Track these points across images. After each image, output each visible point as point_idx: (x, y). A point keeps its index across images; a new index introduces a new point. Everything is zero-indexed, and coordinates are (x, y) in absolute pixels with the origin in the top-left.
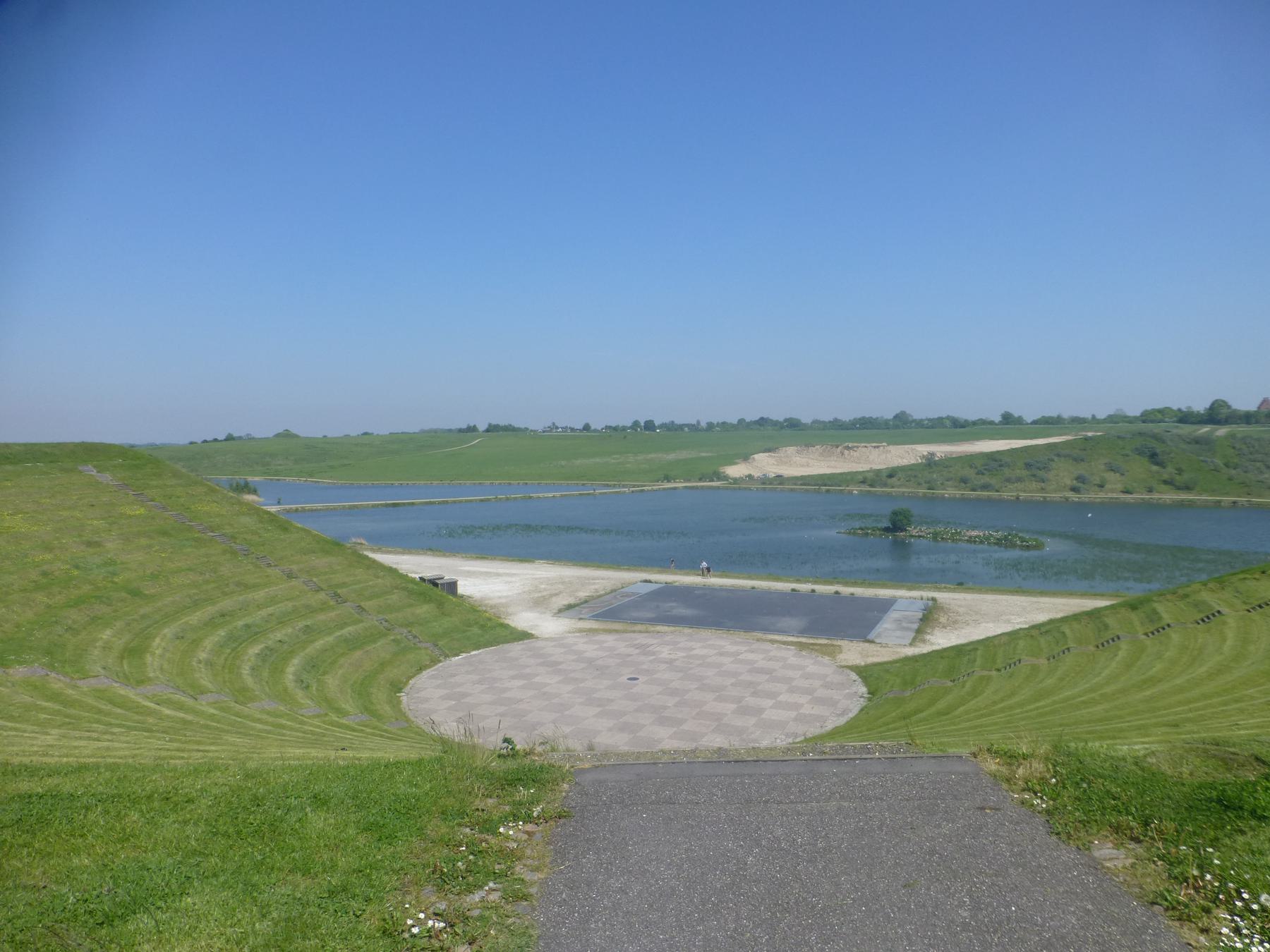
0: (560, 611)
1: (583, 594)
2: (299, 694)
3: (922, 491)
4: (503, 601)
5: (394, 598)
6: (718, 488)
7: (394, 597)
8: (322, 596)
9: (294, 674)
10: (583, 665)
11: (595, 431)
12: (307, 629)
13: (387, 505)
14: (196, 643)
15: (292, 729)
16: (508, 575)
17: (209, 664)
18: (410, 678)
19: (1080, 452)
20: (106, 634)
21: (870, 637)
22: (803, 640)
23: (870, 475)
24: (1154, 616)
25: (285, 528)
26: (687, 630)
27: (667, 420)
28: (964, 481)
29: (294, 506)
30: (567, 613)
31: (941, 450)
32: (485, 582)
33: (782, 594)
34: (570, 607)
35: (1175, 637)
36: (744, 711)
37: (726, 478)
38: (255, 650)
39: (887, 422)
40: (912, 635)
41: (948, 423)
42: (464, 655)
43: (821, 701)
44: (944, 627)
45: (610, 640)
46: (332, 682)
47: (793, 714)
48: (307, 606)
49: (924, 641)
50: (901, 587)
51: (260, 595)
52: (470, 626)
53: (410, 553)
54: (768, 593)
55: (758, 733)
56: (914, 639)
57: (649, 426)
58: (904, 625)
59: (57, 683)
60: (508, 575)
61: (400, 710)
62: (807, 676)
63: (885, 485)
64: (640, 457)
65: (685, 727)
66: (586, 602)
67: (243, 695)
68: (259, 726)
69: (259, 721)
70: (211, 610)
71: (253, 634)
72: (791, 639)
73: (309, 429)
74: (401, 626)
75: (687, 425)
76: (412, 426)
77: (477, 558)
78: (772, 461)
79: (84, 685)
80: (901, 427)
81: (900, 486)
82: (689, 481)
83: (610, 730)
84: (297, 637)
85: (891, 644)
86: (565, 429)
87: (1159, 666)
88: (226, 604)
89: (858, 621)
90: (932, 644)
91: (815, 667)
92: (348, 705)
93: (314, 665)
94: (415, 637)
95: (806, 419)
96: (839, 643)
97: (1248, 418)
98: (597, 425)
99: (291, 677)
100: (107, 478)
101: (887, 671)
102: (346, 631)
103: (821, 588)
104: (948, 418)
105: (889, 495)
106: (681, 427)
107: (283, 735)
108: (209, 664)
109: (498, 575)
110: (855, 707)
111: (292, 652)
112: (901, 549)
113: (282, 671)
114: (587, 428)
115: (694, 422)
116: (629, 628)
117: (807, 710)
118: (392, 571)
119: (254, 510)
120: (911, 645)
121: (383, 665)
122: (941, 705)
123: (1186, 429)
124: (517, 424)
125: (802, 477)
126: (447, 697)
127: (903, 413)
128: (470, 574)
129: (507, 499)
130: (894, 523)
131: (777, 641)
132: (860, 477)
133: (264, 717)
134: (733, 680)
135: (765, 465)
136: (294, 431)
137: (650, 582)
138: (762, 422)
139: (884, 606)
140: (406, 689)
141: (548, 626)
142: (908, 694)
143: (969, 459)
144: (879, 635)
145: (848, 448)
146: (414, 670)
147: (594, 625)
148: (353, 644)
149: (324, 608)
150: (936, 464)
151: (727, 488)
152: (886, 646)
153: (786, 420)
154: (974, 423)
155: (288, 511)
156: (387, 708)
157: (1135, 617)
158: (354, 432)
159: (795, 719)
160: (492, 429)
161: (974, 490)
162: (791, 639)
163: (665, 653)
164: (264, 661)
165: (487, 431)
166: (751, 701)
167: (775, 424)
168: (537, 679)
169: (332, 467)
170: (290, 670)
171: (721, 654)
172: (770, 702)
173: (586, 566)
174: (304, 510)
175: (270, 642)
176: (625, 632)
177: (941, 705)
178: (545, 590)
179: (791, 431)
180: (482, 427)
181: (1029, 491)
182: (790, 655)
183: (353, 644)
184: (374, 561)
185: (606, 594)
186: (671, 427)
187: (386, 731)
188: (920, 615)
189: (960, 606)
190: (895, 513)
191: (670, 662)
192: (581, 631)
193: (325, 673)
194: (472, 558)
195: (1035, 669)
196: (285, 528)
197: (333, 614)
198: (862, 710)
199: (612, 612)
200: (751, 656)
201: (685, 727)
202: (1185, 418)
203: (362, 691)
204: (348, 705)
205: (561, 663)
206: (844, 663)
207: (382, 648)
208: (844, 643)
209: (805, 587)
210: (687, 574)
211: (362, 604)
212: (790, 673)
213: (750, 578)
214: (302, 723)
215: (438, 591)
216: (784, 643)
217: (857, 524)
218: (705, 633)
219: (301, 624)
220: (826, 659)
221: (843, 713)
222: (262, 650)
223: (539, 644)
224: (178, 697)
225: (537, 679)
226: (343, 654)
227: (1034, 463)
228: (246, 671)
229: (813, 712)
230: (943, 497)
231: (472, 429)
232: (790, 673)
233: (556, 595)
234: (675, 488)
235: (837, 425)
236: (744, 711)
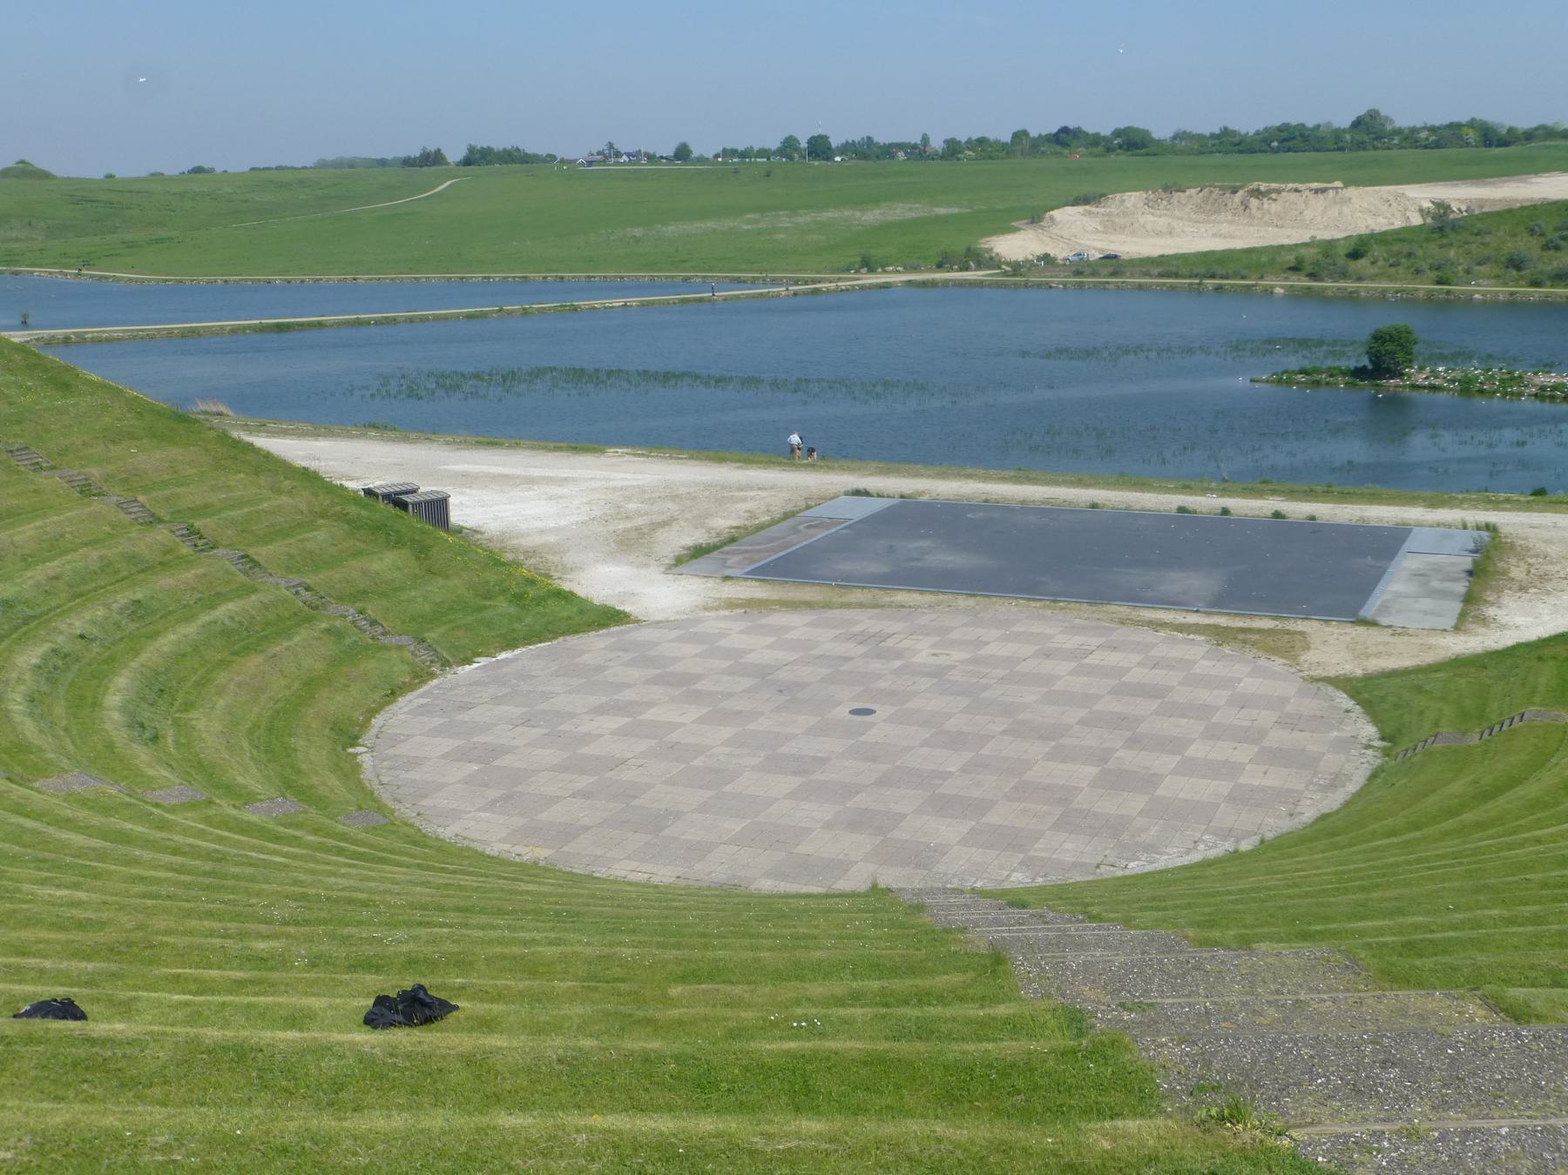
0: (679, 561)
1: (723, 523)
2: (142, 755)
3: (1424, 287)
4: (552, 539)
5: (321, 536)
6: (979, 284)
7: (321, 535)
8: (161, 534)
9: (123, 709)
10: (747, 682)
11: (702, 160)
12: (137, 610)
13: (262, 329)
15: (147, 844)
16: (550, 480)
18: (373, 712)
21: (1367, 611)
22: (1222, 621)
23: (1309, 254)
25: (63, 383)
26: (963, 602)
27: (856, 136)
28: (1516, 263)
29: (60, 332)
30: (697, 564)
31: (1461, 196)
32: (509, 497)
33: (1157, 519)
34: (698, 552)
36: (1116, 781)
37: (993, 262)
38: (29, 657)
39: (1338, 135)
40: (1457, 606)
41: (1471, 135)
42: (483, 661)
44: (1523, 589)
45: (797, 624)
46: (207, 725)
47: (1225, 787)
48: (132, 558)
49: (1484, 621)
50: (1411, 501)
52: (488, 596)
53: (329, 434)
54: (1129, 517)
55: (1154, 830)
56: (1462, 616)
57: (819, 148)
58: (1435, 584)
60: (550, 480)
61: (361, 786)
62: (1243, 702)
63: (1344, 275)
64: (805, 218)
65: (993, 818)
66: (733, 540)
68: (78, 839)
69: (68, 823)
72: (1193, 619)
74: (340, 599)
75: (900, 146)
76: (301, 153)
77: (478, 444)
78: (1092, 224)
80: (1367, 147)
81: (1372, 278)
82: (915, 268)
83: (828, 826)
84: (118, 625)
85: (1413, 627)
86: (635, 156)
89: (1337, 578)
90: (1503, 627)
91: (1254, 677)
93: (158, 688)
94: (373, 623)
95: (1161, 131)
96: (1300, 626)
99: (116, 716)
101: (1419, 689)
102: (226, 610)
103: (1242, 506)
104: (1472, 124)
105: (1351, 298)
106: (889, 151)
107: (135, 862)
109: (530, 481)
110: (1357, 769)
111: (110, 660)
112: (1392, 416)
113: (96, 704)
114: (682, 153)
115: (917, 140)
116: (835, 596)
117: (1253, 777)
118: (309, 477)
120: (1457, 628)
121: (311, 685)
124: (530, 148)
125: (1162, 260)
126: (462, 755)
127: (1373, 115)
129: (525, 312)
130: (1376, 358)
131: (1164, 625)
132: (1290, 259)
133: (82, 814)
134: (1082, 713)
135: (1075, 232)
136: (40, 162)
137: (866, 493)
138: (1065, 138)
139: (1389, 542)
140: (368, 738)
141: (659, 595)
142: (1474, 740)
143: (1529, 217)
144: (1384, 609)
145: (1257, 193)
146: (377, 696)
147: (757, 591)
148: (241, 639)
149: (166, 561)
150: (1456, 226)
151: (998, 285)
152: (1403, 632)
153: (1118, 133)
154: (1529, 136)
155: (49, 343)
156: (333, 781)
158: (174, 164)
159: (1231, 799)
160: (477, 158)
161: (1536, 284)
162: (1193, 619)
163: (923, 652)
164: (52, 681)
165: (467, 162)
166: (1127, 758)
167: (1095, 140)
168: (650, 715)
169: (131, 245)
170: (113, 700)
171: (1047, 655)
172: (1169, 762)
173: (720, 460)
174: (82, 340)
175: (60, 639)
176: (827, 606)
178: (638, 513)
180: (454, 154)
182: (1196, 651)
183: (241, 639)
184: (268, 456)
185: (773, 523)
186: (865, 151)
187: (342, 837)
188: (1467, 562)
189: (1549, 542)
190: (1379, 338)
191: (938, 673)
192: (731, 604)
193: (188, 706)
194: (467, 445)
196: (63, 383)
197: (190, 575)
198: (1373, 776)
199: (790, 561)
200: (1113, 659)
201: (993, 818)
203: (273, 739)
204: (251, 780)
205: (699, 677)
206: (1319, 672)
207: (304, 650)
208: (1310, 627)
209: (1206, 503)
210: (943, 476)
211: (252, 552)
212: (1204, 696)
213: (1080, 483)
214: (163, 825)
215: (410, 518)
216: (1181, 628)
217: (1293, 362)
218: (1005, 607)
219: (123, 598)
220: (1278, 663)
221: (1335, 782)
222: (45, 658)
223: (644, 634)
225: (650, 715)
226: (223, 664)
228: (17, 705)
229: (1268, 782)
230: (1469, 300)
231: (432, 159)
233: (664, 524)
234: (887, 286)
235: (1229, 144)
236: (1116, 781)
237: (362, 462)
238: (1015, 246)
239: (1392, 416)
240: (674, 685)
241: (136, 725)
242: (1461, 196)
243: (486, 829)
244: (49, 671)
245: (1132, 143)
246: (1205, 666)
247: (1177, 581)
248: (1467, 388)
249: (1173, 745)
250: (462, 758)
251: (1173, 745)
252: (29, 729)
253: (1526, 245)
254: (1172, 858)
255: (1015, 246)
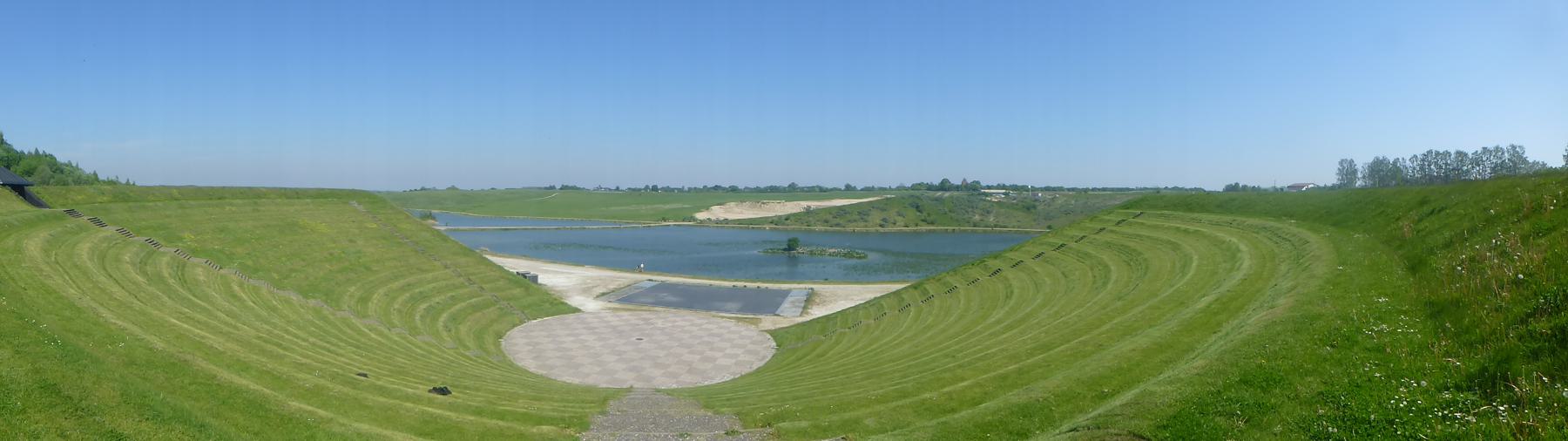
2: (445, 334)
14: (394, 299)
17: (399, 311)
19: (883, 206)
20: (352, 289)
24: (925, 292)
31: (814, 204)
32: (555, 277)
33: (728, 289)
35: (937, 302)
36: (706, 359)
43: (750, 352)
46: (463, 329)
51: (430, 276)
57: (655, 188)
59: (327, 311)
62: (742, 337)
67: (414, 331)
70: (402, 282)
71: (423, 297)
73: (464, 186)
79: (340, 314)
80: (792, 192)
85: (789, 316)
87: (931, 319)
88: (411, 279)
89: (768, 303)
92: (471, 344)
93: (454, 318)
95: (741, 187)
97: (957, 188)
98: (623, 187)
100: (361, 208)
103: (749, 285)
108: (399, 311)
112: (793, 261)
118: (501, 268)
119: (429, 229)
122: (819, 351)
123: (931, 193)
128: (546, 272)
135: (718, 212)
138: (716, 188)
139: (785, 294)
141: (590, 305)
143: (829, 210)
147: (617, 305)
148: (476, 308)
157: (916, 293)
160: (564, 188)
163: (660, 323)
166: (709, 353)
177: (819, 351)
179: (734, 193)
181: (859, 228)
182: (732, 324)
183: (476, 308)
186: (667, 190)
195: (868, 326)
199: (628, 298)
202: (930, 188)
203: (479, 337)
209: (740, 284)
224: (382, 328)
227: (862, 212)
231: (552, 188)
232: (736, 351)
235: (758, 190)
236: (706, 359)
237: (515, 265)
238: (701, 216)
239: (793, 261)
240: (587, 326)
241: (446, 327)
242: (814, 204)
243: (530, 364)
244: (427, 310)
245: (734, 189)
246: (734, 329)
247: (730, 305)
248: (812, 253)
249: (721, 350)
250: (531, 347)
251: (721, 350)
252: (419, 323)
253: (829, 217)
254: (717, 380)
255: (701, 216)
